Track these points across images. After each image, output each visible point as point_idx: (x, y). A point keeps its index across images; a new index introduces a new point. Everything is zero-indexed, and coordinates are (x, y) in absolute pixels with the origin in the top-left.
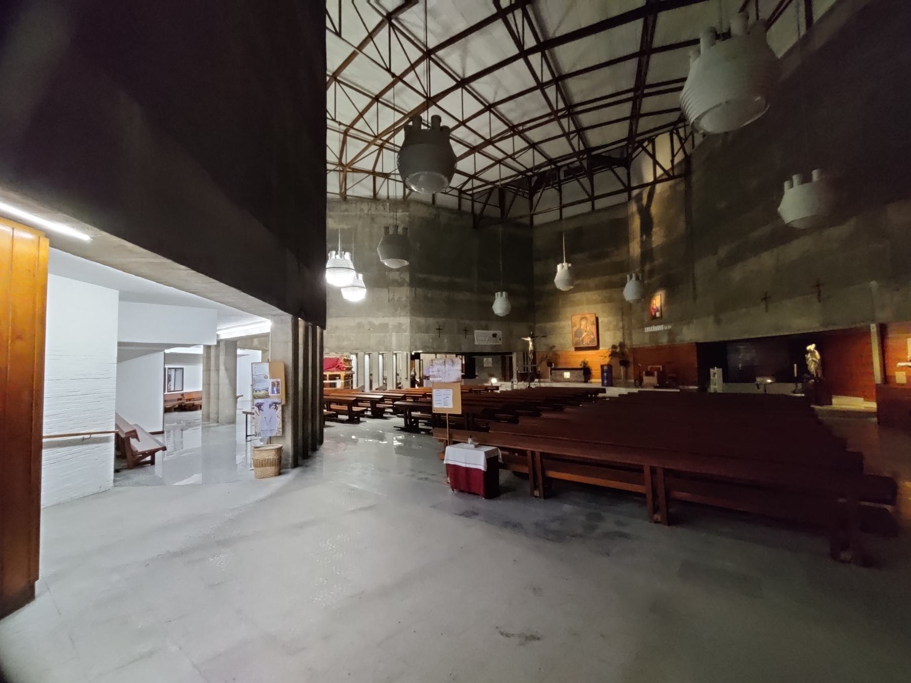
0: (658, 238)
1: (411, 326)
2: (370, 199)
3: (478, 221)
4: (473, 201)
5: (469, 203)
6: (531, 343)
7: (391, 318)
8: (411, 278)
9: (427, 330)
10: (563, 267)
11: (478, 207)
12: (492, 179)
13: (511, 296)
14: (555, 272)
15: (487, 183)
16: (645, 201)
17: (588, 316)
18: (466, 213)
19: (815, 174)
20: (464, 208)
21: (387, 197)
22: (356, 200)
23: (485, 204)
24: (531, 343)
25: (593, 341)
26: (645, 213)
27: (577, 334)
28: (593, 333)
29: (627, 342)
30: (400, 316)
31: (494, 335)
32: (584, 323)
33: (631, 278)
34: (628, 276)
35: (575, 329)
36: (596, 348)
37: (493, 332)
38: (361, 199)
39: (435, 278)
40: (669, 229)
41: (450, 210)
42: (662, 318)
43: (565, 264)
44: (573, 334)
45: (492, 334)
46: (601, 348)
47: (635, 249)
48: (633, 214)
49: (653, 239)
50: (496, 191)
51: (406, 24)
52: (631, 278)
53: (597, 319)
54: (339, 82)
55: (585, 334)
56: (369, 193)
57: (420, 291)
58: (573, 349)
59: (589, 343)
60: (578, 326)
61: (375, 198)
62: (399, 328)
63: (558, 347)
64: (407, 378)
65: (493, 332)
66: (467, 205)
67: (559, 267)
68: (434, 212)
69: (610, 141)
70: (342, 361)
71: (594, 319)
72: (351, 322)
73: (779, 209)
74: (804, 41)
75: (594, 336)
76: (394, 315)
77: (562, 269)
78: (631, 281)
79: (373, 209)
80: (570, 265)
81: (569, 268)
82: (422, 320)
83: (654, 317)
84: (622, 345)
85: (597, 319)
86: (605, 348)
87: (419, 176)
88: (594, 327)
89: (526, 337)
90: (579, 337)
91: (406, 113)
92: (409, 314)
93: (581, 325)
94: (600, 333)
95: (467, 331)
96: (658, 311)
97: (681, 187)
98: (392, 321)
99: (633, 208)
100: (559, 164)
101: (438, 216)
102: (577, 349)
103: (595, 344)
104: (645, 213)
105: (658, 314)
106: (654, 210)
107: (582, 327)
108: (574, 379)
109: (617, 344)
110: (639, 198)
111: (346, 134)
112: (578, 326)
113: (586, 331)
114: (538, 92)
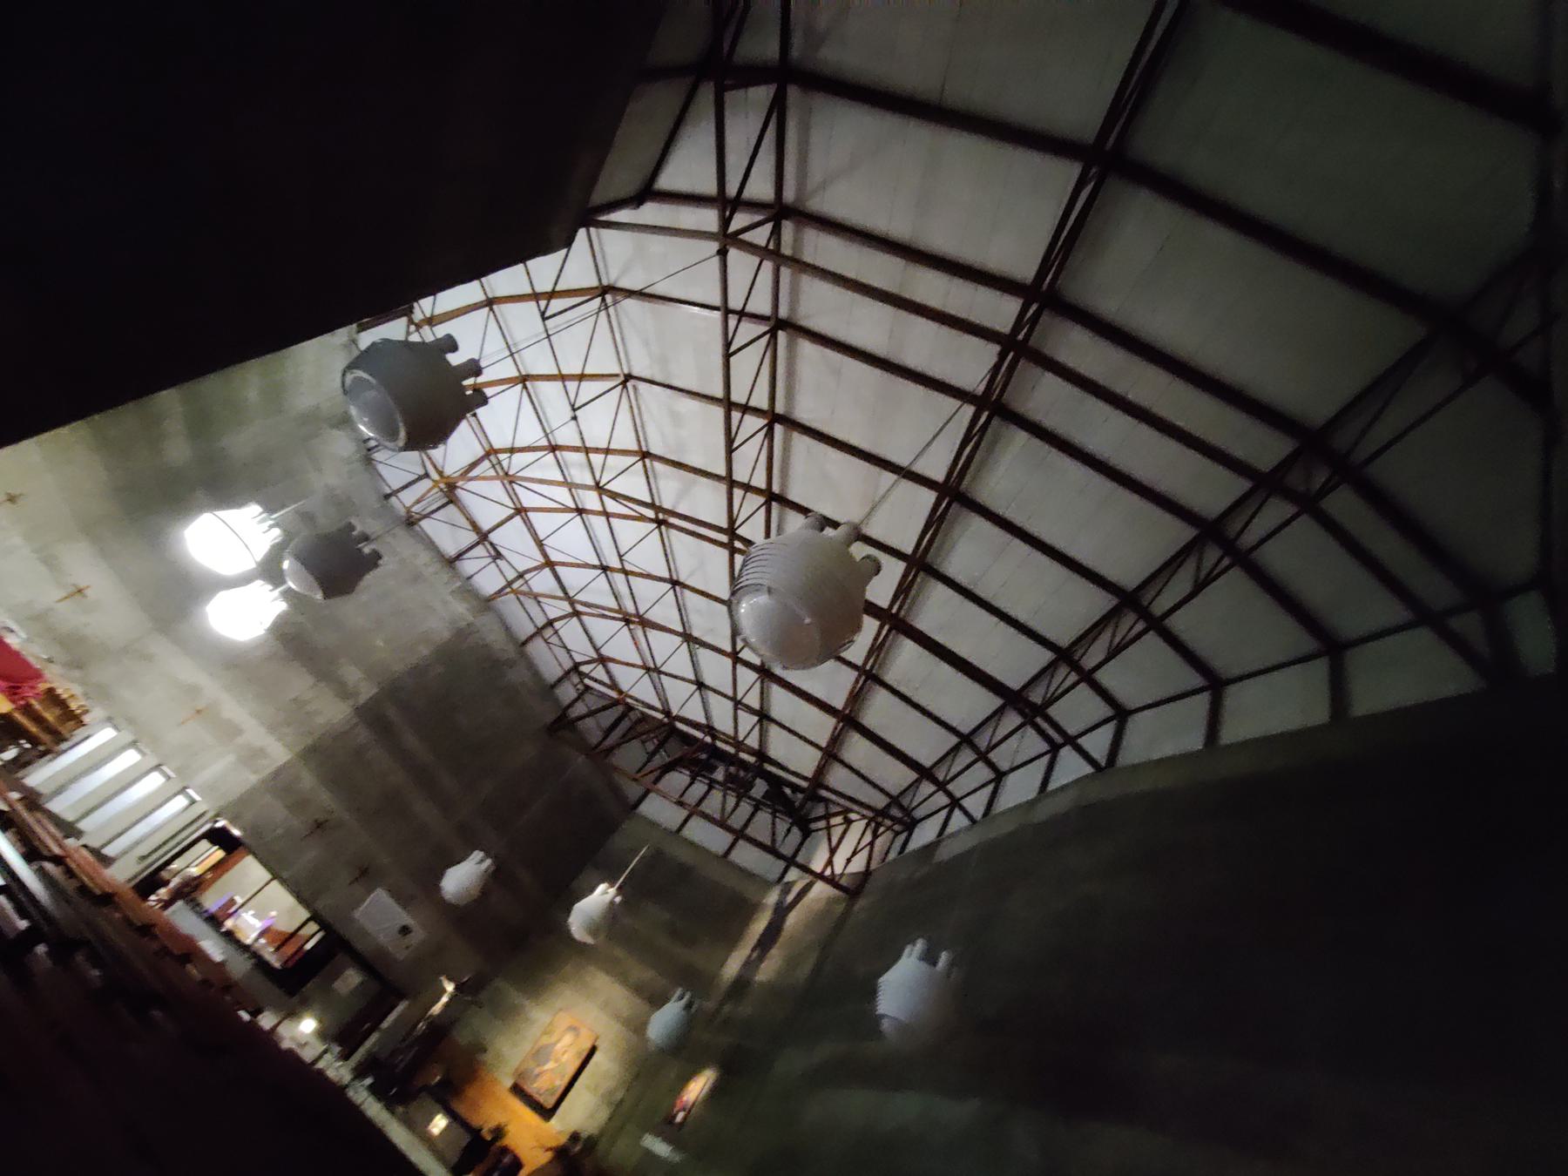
0: (767, 971)
1: (277, 773)
2: (443, 556)
3: (563, 723)
4: (580, 697)
5: (573, 695)
6: (445, 999)
7: (263, 730)
8: (374, 701)
9: (298, 804)
10: (605, 892)
11: (580, 709)
12: (624, 687)
13: (495, 879)
14: (592, 890)
15: (614, 685)
16: (790, 898)
17: (584, 1031)
18: (556, 701)
19: (944, 957)
20: (559, 691)
21: (469, 575)
22: (423, 539)
23: (591, 714)
24: (445, 999)
25: (551, 1091)
26: (781, 911)
27: (540, 1054)
28: (564, 1076)
29: (601, 1147)
30: (279, 739)
31: (405, 930)
32: (568, 1039)
33: (681, 998)
34: (679, 992)
35: (545, 1040)
36: (546, 1113)
37: (407, 919)
38: (431, 545)
39: (410, 740)
40: (792, 963)
41: (536, 674)
42: (680, 1129)
43: (612, 891)
44: (536, 1047)
45: (404, 923)
46: (553, 1121)
47: (732, 967)
48: (765, 905)
49: (763, 965)
50: (620, 708)
51: (641, 402)
52: (681, 998)
53: (593, 1050)
54: (525, 387)
55: (550, 1065)
56: (451, 550)
57: (364, 735)
58: (509, 1083)
59: (542, 1092)
60: (553, 1039)
61: (452, 562)
62: (252, 756)
63: (488, 1057)
64: (143, 858)
65: (407, 919)
66: (567, 693)
67: (602, 887)
68: (511, 651)
69: (792, 768)
70: (42, 687)
71: (587, 1046)
72: (188, 671)
73: (881, 980)
74: (1031, 804)
75: (561, 1083)
76: (272, 728)
77: (602, 895)
78: (676, 1003)
79: (431, 570)
80: (618, 899)
81: (612, 902)
82: (308, 780)
83: (670, 1119)
84: (591, 1144)
85: (593, 1050)
86: (559, 1128)
87: (371, 387)
88: (577, 1063)
89: (450, 979)
90: (538, 1065)
91: (569, 481)
92: (298, 749)
93: (558, 1041)
94: (577, 1085)
95: (366, 875)
96: (684, 1110)
97: (840, 908)
98: (255, 733)
99: (772, 898)
100: (719, 744)
101: (511, 664)
102: (517, 1090)
103: (549, 1102)
104: (781, 911)
105: (680, 1117)
106: (792, 919)
107: (559, 1046)
108: (440, 1146)
109: (584, 1135)
110: (788, 888)
111: (487, 455)
112: (553, 1039)
113: (557, 1061)
114: (552, 338)
